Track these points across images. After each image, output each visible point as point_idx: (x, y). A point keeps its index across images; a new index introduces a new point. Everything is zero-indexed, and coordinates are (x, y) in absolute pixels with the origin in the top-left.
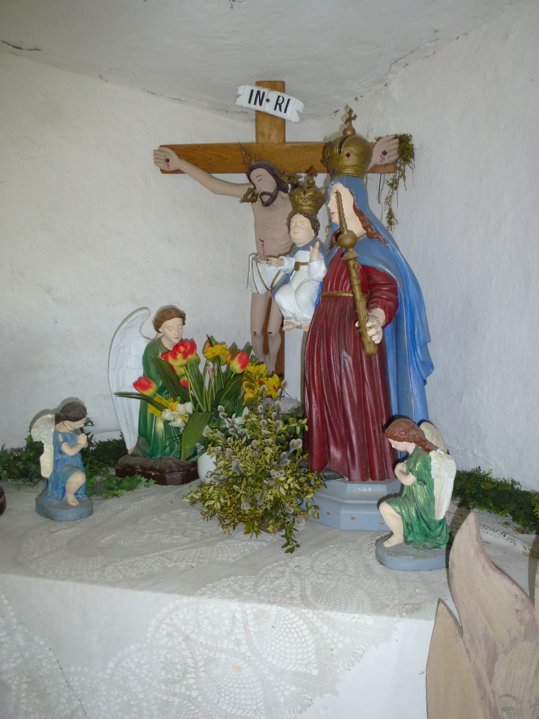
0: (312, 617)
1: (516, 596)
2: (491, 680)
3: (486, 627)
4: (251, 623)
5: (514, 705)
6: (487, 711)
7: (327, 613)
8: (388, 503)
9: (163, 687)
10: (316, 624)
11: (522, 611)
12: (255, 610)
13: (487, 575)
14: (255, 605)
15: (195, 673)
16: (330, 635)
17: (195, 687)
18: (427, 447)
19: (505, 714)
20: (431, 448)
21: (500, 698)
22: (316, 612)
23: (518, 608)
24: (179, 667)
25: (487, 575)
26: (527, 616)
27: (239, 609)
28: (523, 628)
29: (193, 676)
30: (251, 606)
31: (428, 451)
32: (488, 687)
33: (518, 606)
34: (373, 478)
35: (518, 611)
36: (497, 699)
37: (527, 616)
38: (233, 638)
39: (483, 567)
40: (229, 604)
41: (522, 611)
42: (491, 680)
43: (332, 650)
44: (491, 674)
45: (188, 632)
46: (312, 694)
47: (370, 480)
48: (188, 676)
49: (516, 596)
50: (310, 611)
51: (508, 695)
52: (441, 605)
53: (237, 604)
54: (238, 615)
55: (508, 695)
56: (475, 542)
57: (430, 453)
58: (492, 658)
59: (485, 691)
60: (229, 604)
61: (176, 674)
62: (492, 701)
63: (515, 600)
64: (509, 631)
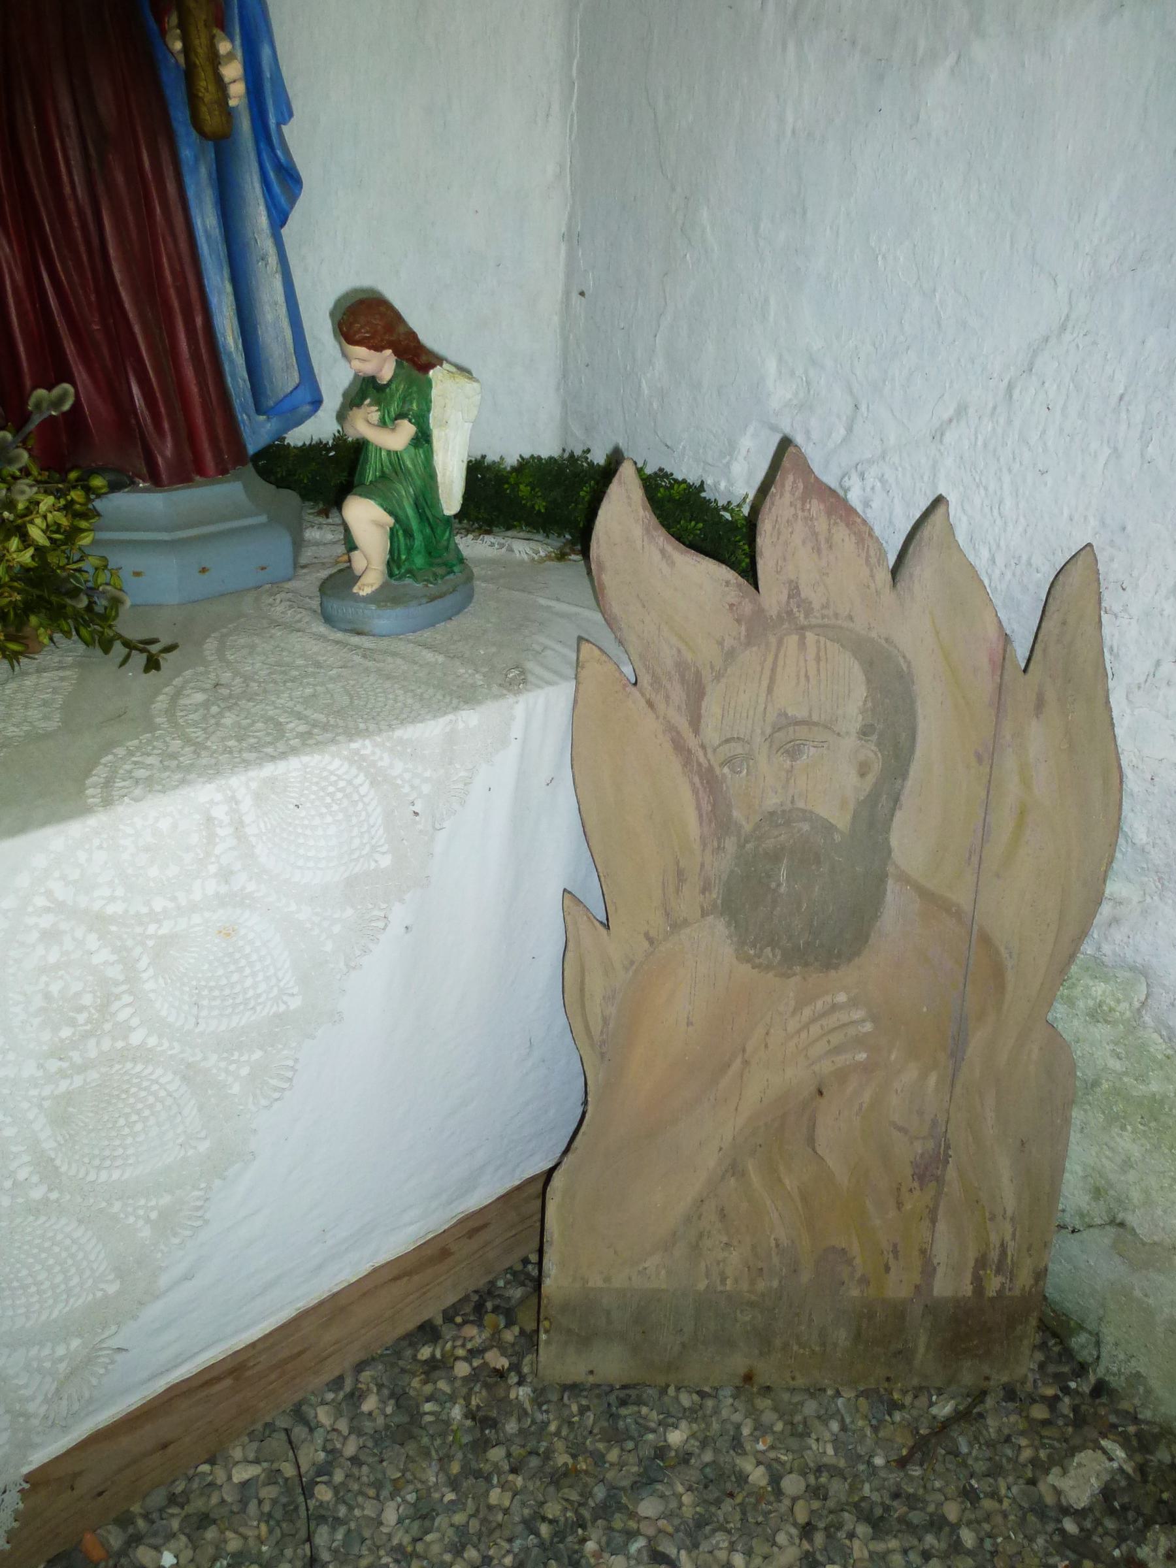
0: (374, 753)
1: (728, 583)
2: (696, 732)
3: (679, 651)
4: (247, 819)
5: (739, 750)
6: (696, 780)
7: (398, 733)
8: (360, 495)
9: (53, 1065)
10: (380, 764)
11: (740, 603)
12: (254, 785)
13: (672, 564)
14: (252, 774)
15: (130, 992)
16: (407, 776)
17: (135, 1022)
18: (424, 359)
19: (726, 770)
20: (434, 361)
21: (715, 750)
22: (378, 739)
23: (733, 601)
24: (87, 999)
25: (672, 564)
26: (747, 608)
27: (219, 797)
28: (743, 628)
29: (127, 999)
30: (243, 778)
31: (426, 368)
32: (692, 742)
33: (732, 596)
34: (201, 471)
35: (732, 605)
36: (710, 755)
37: (747, 608)
38: (213, 869)
39: (663, 552)
40: (192, 794)
41: (740, 603)
42: (696, 732)
43: (413, 804)
44: (695, 722)
45: (97, 906)
46: (384, 906)
47: (198, 478)
48: (116, 1005)
49: (728, 583)
50: (367, 742)
51: (727, 741)
52: (585, 647)
53: (210, 787)
54: (220, 812)
55: (727, 741)
56: (641, 512)
57: (431, 372)
58: (696, 694)
59: (689, 751)
60: (192, 794)
61: (81, 1018)
62: (702, 759)
63: (727, 589)
64: (721, 643)
